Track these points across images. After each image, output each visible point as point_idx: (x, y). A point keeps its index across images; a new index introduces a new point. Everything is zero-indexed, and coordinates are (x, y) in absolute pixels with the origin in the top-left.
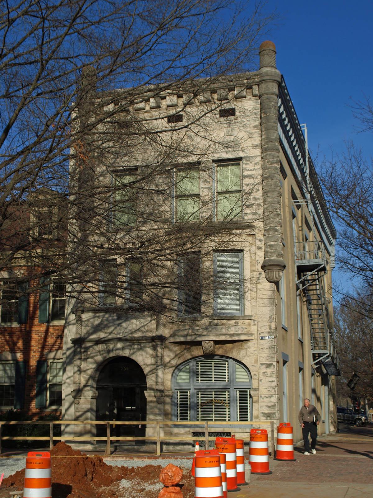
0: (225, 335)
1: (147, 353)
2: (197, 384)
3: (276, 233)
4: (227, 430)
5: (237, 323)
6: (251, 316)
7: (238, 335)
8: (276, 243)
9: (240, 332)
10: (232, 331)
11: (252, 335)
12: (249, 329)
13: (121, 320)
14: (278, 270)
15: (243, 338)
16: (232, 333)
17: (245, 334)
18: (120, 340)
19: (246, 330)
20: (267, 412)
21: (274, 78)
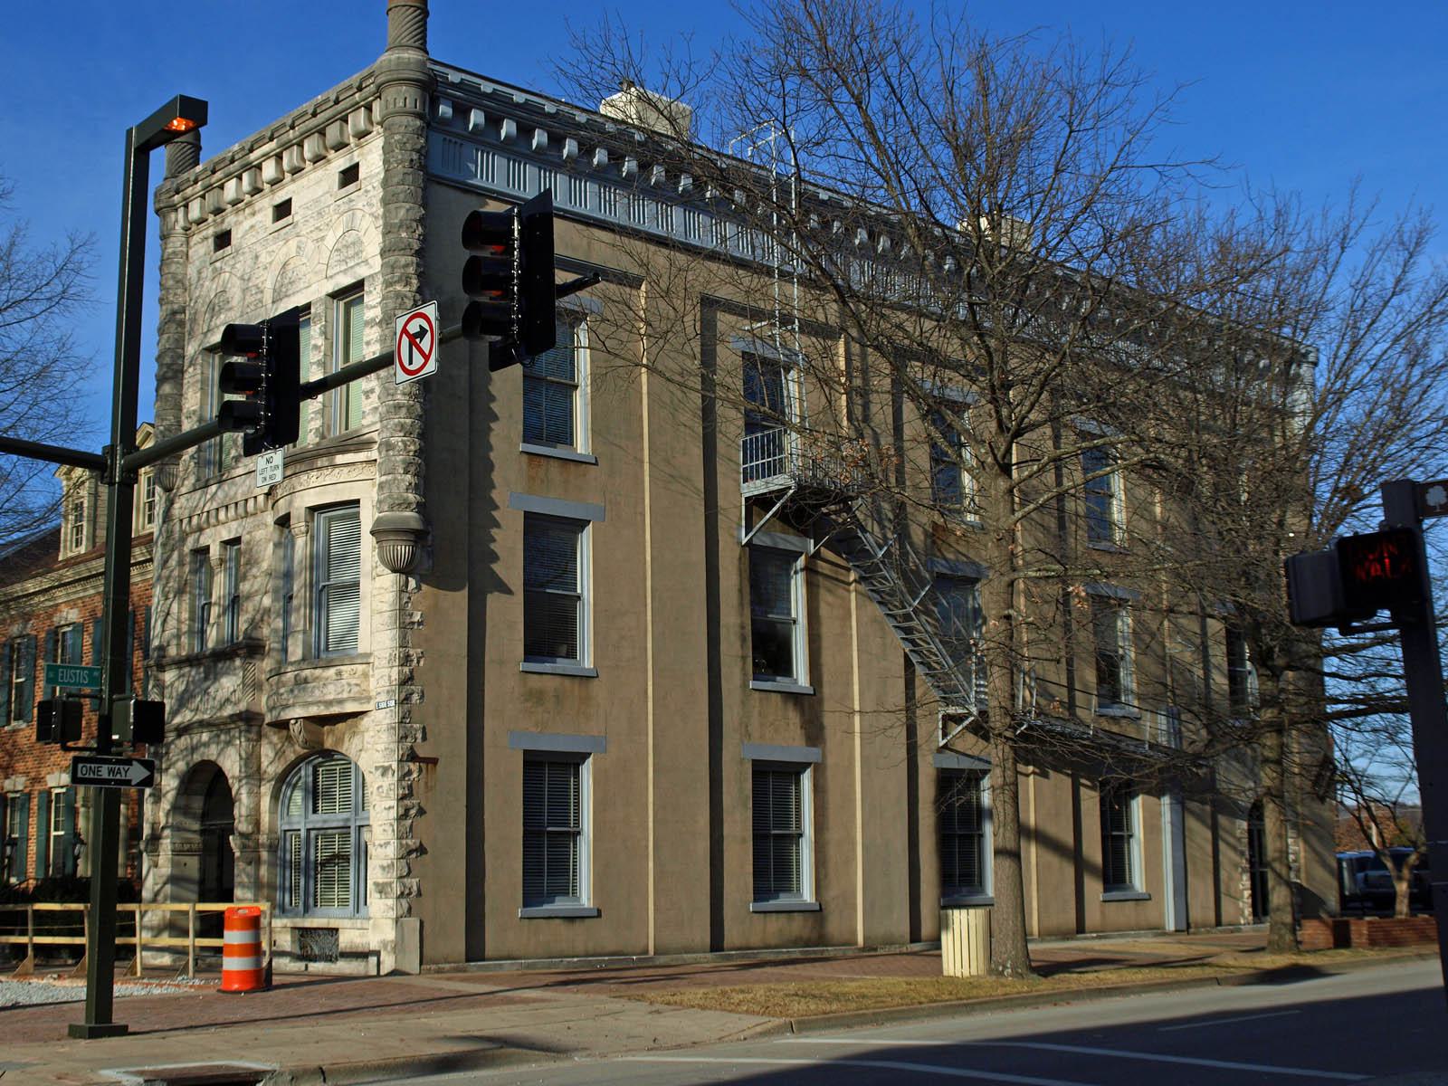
0: (318, 703)
1: (172, 742)
2: (314, 817)
3: (391, 453)
4: (1045, 985)
5: (339, 674)
6: (369, 655)
7: (341, 702)
8: (390, 477)
9: (345, 695)
10: (331, 693)
11: (369, 699)
12: (363, 687)
13: (1370, 828)
14: (392, 543)
15: (350, 708)
16: (331, 697)
17: (354, 699)
18: (203, 725)
19: (355, 689)
20: (381, 881)
21: (395, 76)
